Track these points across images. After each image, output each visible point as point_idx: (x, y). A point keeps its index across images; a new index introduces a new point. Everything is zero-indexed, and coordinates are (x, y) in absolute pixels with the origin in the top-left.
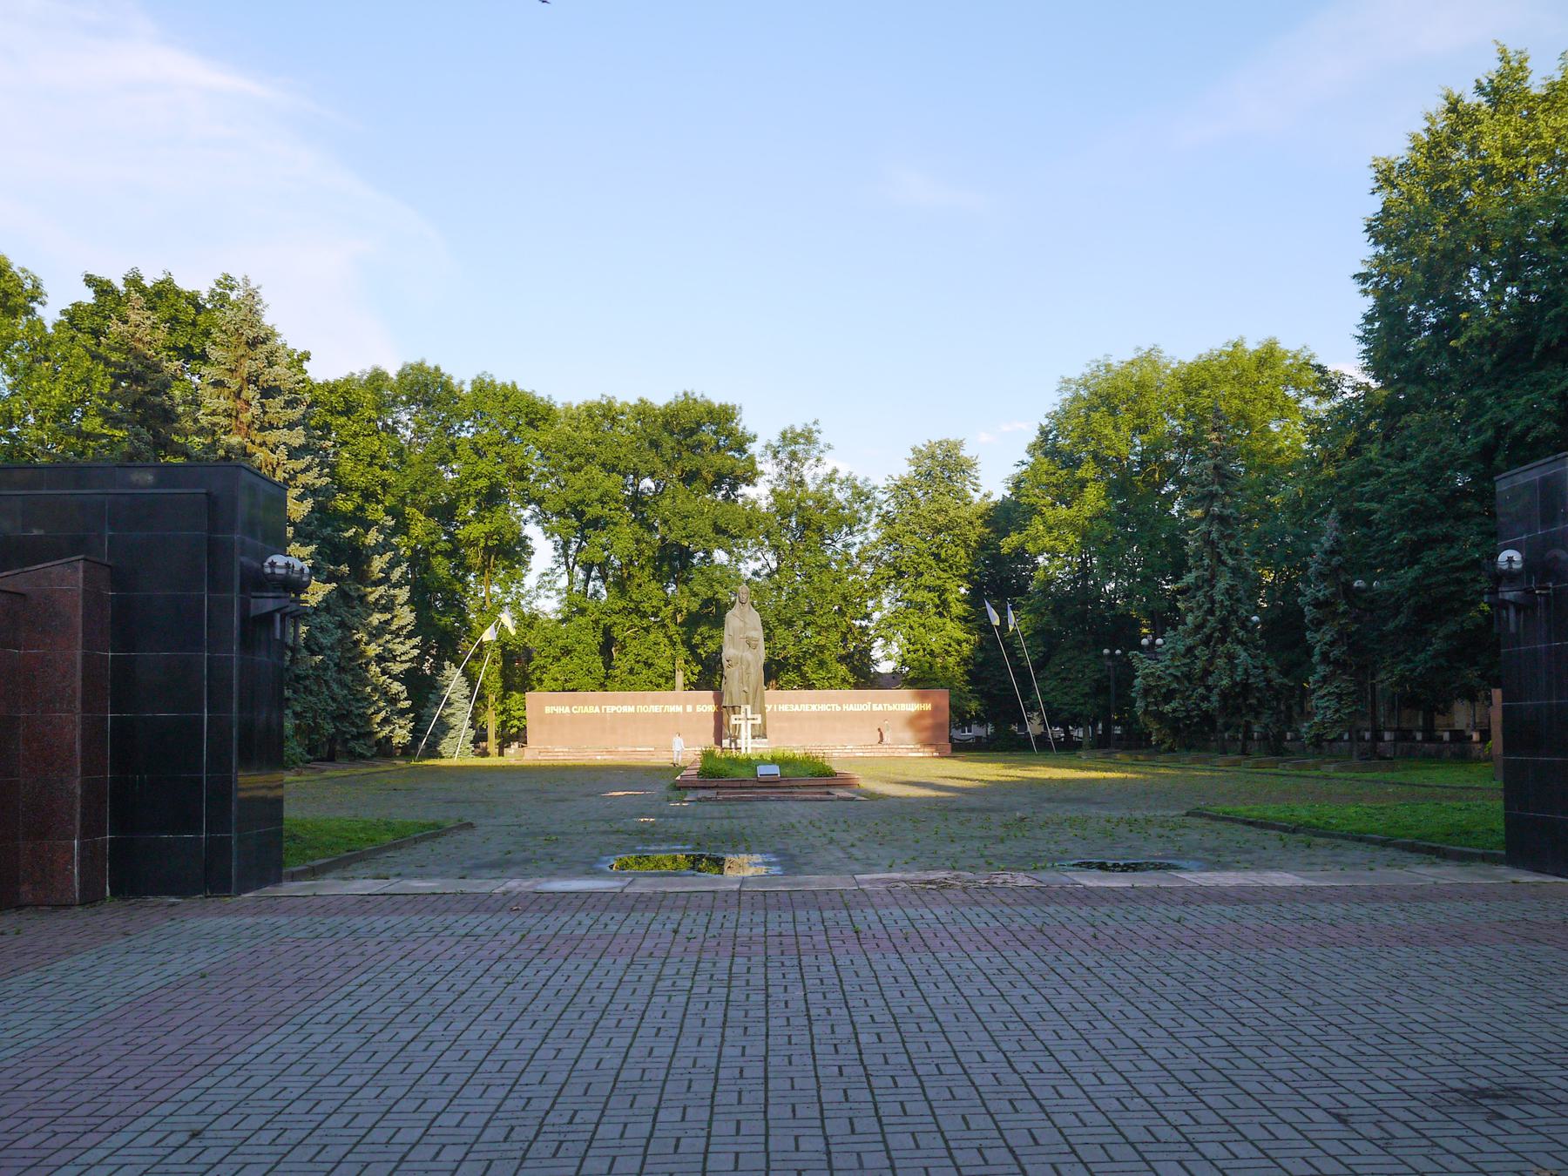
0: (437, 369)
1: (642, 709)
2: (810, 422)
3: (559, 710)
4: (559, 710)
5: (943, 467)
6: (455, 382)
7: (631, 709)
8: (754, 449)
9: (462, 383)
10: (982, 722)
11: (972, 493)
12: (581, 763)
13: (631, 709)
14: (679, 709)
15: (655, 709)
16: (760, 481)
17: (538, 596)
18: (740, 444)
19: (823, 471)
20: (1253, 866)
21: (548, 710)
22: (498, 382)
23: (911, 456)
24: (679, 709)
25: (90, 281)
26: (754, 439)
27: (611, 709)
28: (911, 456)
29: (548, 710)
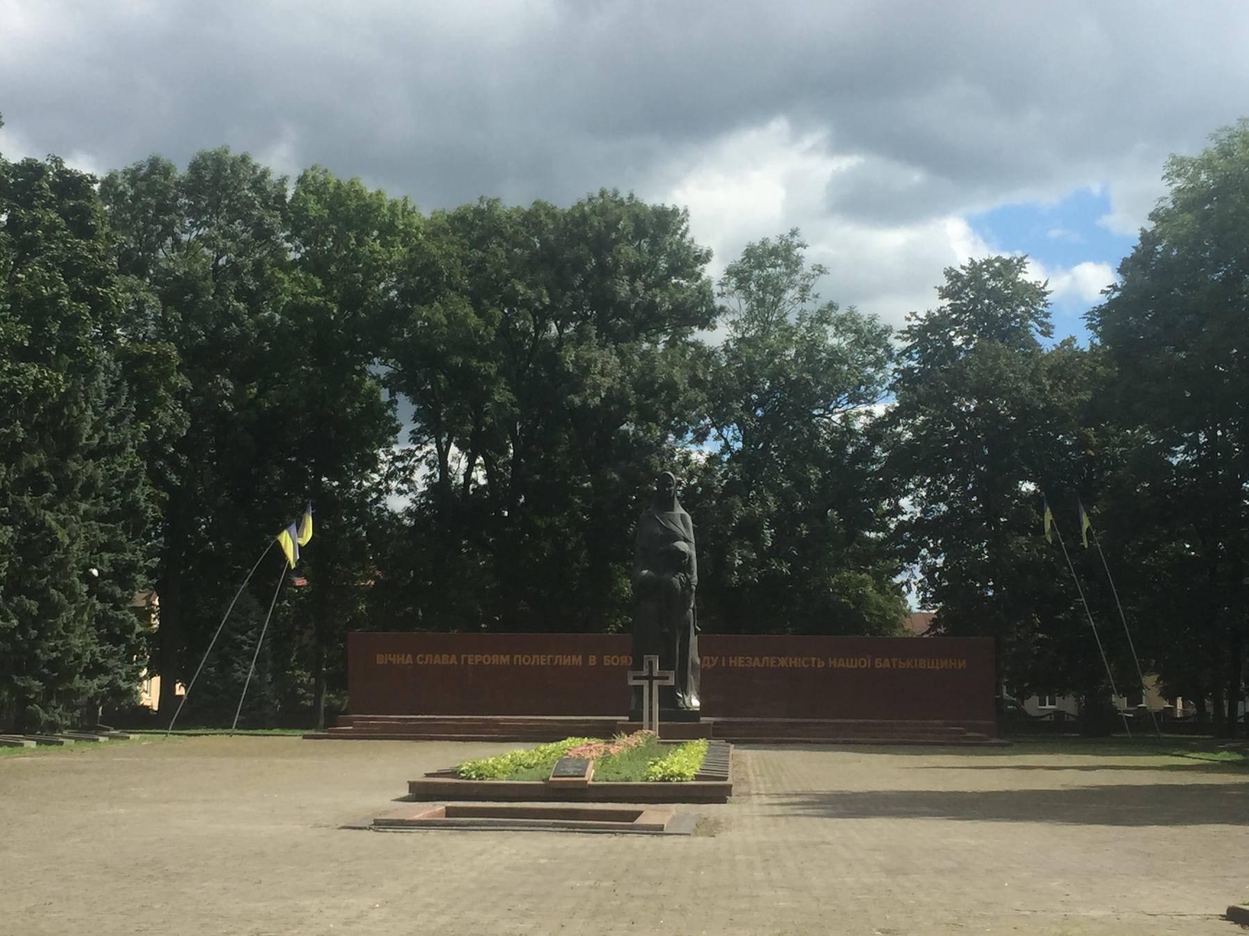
0: (244, 159)
1: (520, 659)
2: (786, 233)
3: (396, 659)
4: (396, 659)
5: (989, 302)
6: (274, 177)
7: (504, 660)
8: (713, 271)
9: (283, 181)
10: (1183, 711)
11: (1039, 339)
12: (1135, 828)
13: (504, 660)
14: (577, 660)
15: (541, 660)
16: (720, 321)
17: (388, 491)
18: (688, 261)
19: (812, 307)
20: (455, 808)
21: (381, 659)
22: (333, 180)
23: (945, 283)
24: (577, 660)
25: (406, 199)
26: (705, 258)
27: (473, 659)
28: (945, 283)
29: (381, 659)
